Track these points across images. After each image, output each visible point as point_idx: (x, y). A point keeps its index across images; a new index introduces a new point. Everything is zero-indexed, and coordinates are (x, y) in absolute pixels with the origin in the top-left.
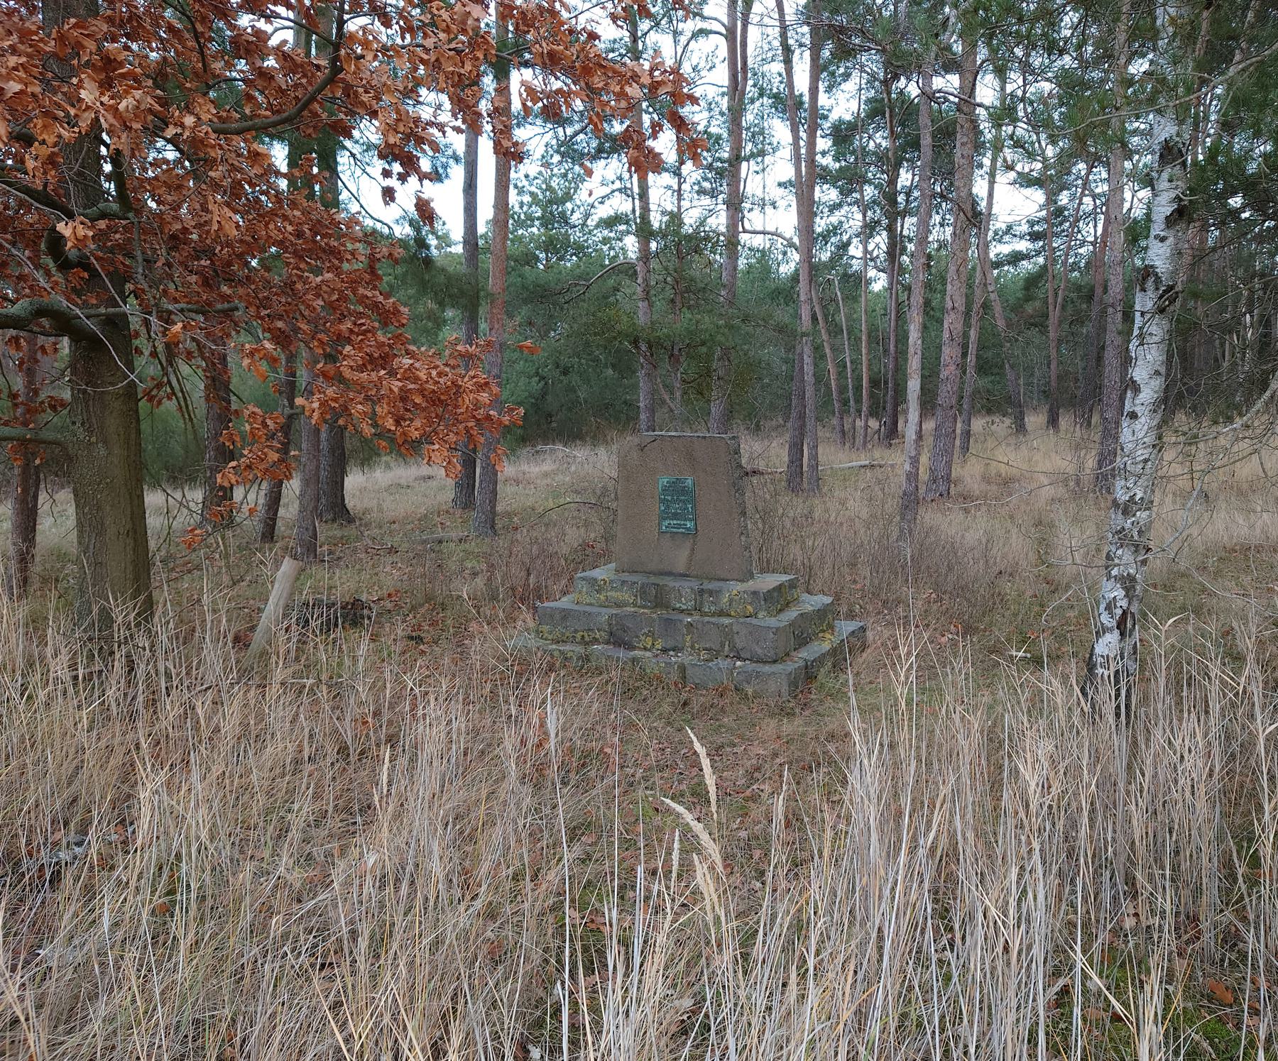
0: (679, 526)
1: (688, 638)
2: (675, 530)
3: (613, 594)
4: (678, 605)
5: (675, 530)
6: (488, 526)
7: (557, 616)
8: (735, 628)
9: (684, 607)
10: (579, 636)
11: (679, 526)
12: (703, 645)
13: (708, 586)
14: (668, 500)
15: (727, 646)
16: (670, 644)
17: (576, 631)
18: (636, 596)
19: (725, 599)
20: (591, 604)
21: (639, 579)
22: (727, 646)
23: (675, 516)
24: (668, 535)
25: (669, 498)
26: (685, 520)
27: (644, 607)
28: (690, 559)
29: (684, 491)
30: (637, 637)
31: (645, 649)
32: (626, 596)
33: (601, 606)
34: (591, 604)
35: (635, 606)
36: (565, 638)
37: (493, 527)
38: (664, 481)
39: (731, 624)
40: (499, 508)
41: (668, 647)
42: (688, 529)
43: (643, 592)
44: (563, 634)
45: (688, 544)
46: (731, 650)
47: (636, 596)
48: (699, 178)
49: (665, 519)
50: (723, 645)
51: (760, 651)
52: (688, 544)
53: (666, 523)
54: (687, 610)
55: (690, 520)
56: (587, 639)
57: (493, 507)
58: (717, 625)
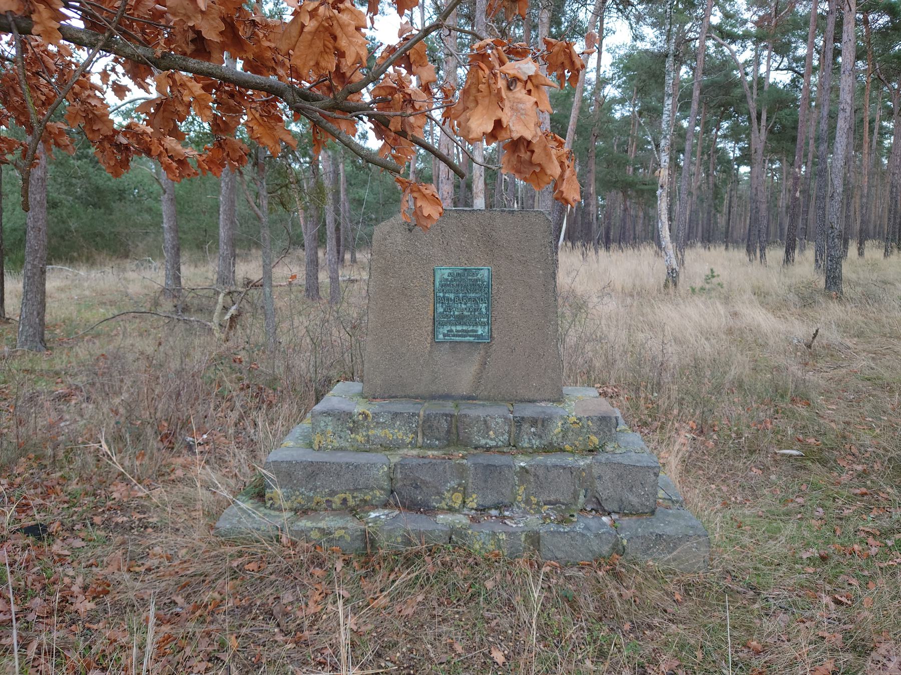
0: (466, 333)
1: (521, 490)
2: (457, 339)
3: (379, 432)
4: (483, 442)
5: (457, 339)
6: (37, 339)
7: (300, 474)
8: (595, 471)
9: (493, 443)
10: (337, 500)
11: (466, 333)
12: (544, 497)
13: (529, 411)
14: (448, 299)
15: (581, 497)
16: (491, 499)
17: (333, 493)
18: (416, 433)
19: (557, 428)
20: (341, 449)
21: (405, 407)
22: (581, 497)
23: (460, 320)
24: (447, 346)
25: (452, 296)
26: (476, 324)
27: (430, 447)
28: (479, 377)
29: (475, 285)
30: (439, 493)
31: (451, 510)
32: (398, 433)
33: (358, 450)
34: (341, 449)
35: (414, 446)
36: (313, 505)
37: (42, 340)
38: (444, 273)
39: (590, 466)
40: (47, 318)
41: (488, 503)
42: (480, 337)
43: (428, 426)
44: (310, 499)
45: (477, 357)
46: (587, 502)
47: (416, 433)
48: (10, 196)
49: (443, 324)
50: (576, 496)
51: (635, 500)
52: (477, 357)
53: (445, 329)
54: (496, 447)
55: (483, 325)
56: (351, 503)
57: (42, 320)
58: (571, 470)
